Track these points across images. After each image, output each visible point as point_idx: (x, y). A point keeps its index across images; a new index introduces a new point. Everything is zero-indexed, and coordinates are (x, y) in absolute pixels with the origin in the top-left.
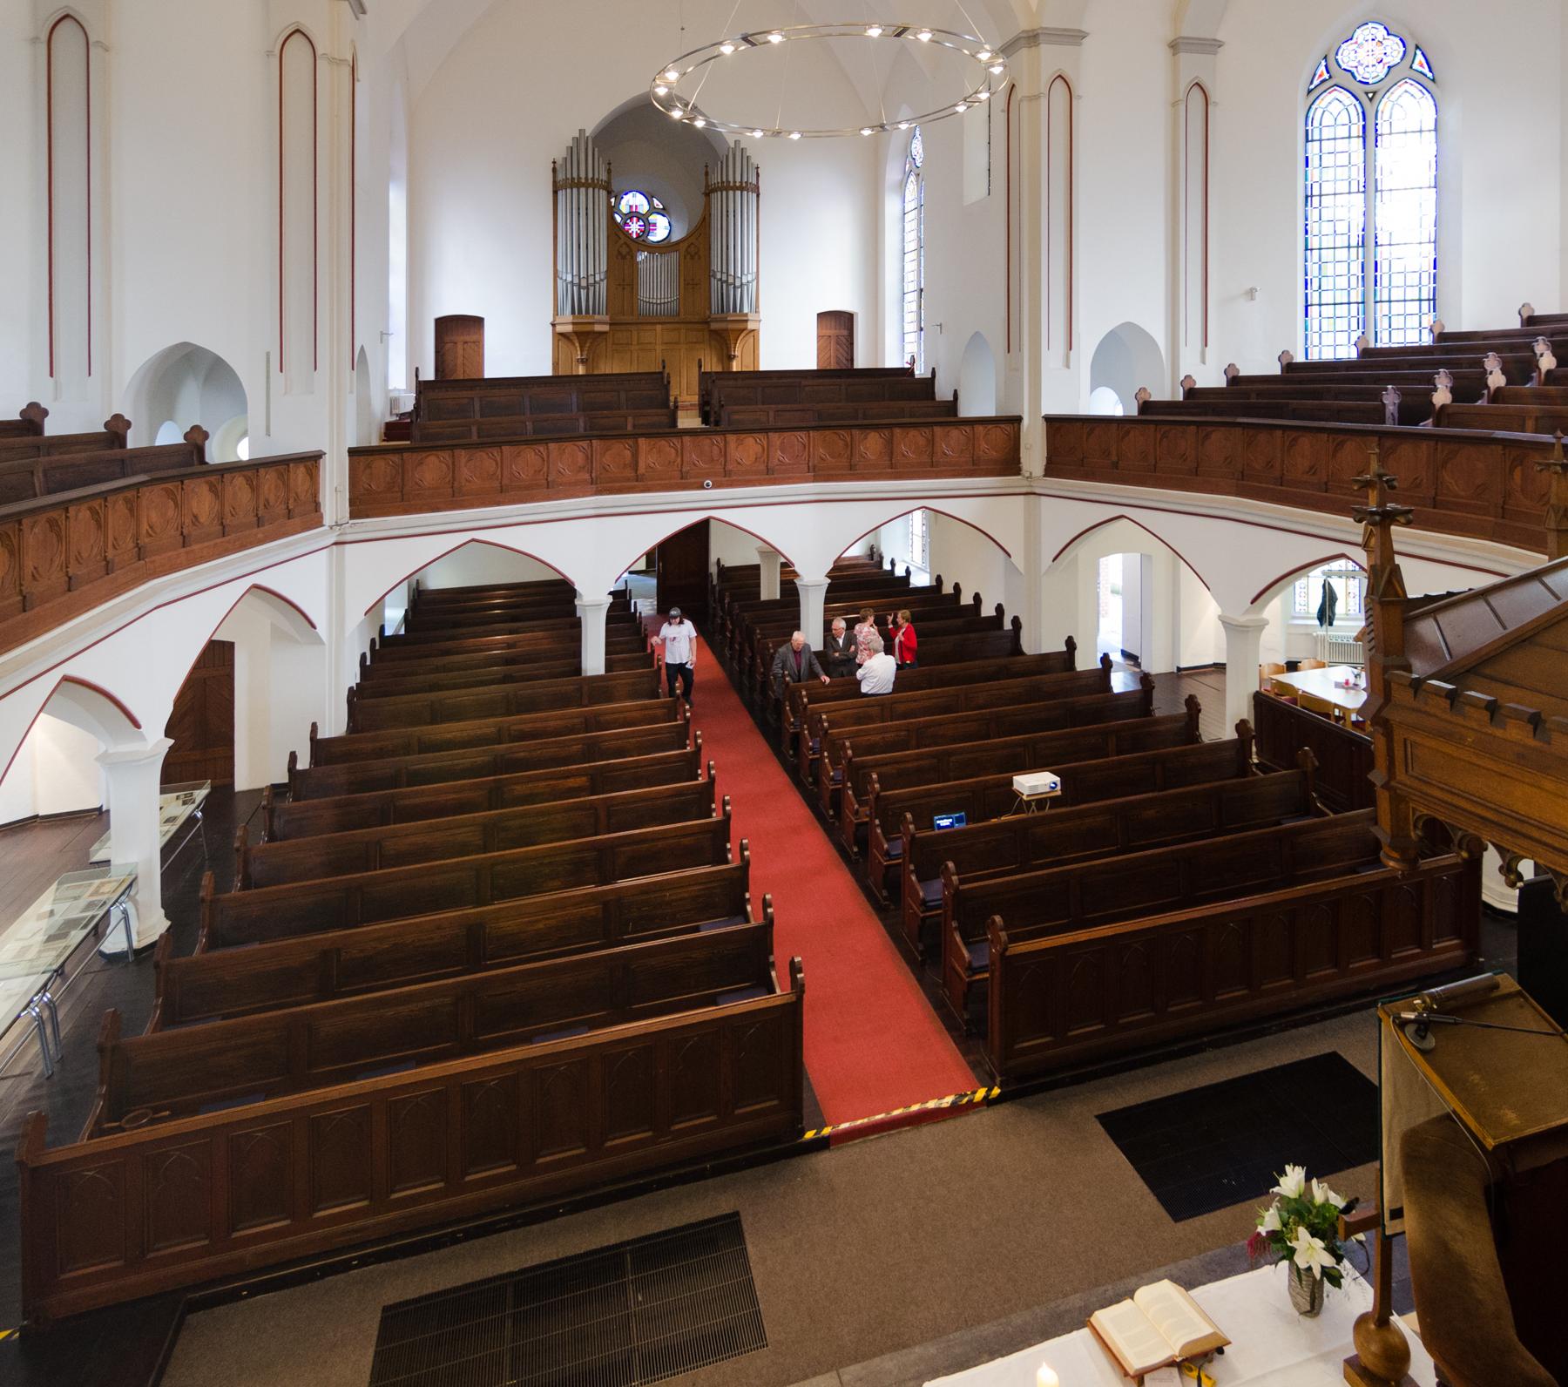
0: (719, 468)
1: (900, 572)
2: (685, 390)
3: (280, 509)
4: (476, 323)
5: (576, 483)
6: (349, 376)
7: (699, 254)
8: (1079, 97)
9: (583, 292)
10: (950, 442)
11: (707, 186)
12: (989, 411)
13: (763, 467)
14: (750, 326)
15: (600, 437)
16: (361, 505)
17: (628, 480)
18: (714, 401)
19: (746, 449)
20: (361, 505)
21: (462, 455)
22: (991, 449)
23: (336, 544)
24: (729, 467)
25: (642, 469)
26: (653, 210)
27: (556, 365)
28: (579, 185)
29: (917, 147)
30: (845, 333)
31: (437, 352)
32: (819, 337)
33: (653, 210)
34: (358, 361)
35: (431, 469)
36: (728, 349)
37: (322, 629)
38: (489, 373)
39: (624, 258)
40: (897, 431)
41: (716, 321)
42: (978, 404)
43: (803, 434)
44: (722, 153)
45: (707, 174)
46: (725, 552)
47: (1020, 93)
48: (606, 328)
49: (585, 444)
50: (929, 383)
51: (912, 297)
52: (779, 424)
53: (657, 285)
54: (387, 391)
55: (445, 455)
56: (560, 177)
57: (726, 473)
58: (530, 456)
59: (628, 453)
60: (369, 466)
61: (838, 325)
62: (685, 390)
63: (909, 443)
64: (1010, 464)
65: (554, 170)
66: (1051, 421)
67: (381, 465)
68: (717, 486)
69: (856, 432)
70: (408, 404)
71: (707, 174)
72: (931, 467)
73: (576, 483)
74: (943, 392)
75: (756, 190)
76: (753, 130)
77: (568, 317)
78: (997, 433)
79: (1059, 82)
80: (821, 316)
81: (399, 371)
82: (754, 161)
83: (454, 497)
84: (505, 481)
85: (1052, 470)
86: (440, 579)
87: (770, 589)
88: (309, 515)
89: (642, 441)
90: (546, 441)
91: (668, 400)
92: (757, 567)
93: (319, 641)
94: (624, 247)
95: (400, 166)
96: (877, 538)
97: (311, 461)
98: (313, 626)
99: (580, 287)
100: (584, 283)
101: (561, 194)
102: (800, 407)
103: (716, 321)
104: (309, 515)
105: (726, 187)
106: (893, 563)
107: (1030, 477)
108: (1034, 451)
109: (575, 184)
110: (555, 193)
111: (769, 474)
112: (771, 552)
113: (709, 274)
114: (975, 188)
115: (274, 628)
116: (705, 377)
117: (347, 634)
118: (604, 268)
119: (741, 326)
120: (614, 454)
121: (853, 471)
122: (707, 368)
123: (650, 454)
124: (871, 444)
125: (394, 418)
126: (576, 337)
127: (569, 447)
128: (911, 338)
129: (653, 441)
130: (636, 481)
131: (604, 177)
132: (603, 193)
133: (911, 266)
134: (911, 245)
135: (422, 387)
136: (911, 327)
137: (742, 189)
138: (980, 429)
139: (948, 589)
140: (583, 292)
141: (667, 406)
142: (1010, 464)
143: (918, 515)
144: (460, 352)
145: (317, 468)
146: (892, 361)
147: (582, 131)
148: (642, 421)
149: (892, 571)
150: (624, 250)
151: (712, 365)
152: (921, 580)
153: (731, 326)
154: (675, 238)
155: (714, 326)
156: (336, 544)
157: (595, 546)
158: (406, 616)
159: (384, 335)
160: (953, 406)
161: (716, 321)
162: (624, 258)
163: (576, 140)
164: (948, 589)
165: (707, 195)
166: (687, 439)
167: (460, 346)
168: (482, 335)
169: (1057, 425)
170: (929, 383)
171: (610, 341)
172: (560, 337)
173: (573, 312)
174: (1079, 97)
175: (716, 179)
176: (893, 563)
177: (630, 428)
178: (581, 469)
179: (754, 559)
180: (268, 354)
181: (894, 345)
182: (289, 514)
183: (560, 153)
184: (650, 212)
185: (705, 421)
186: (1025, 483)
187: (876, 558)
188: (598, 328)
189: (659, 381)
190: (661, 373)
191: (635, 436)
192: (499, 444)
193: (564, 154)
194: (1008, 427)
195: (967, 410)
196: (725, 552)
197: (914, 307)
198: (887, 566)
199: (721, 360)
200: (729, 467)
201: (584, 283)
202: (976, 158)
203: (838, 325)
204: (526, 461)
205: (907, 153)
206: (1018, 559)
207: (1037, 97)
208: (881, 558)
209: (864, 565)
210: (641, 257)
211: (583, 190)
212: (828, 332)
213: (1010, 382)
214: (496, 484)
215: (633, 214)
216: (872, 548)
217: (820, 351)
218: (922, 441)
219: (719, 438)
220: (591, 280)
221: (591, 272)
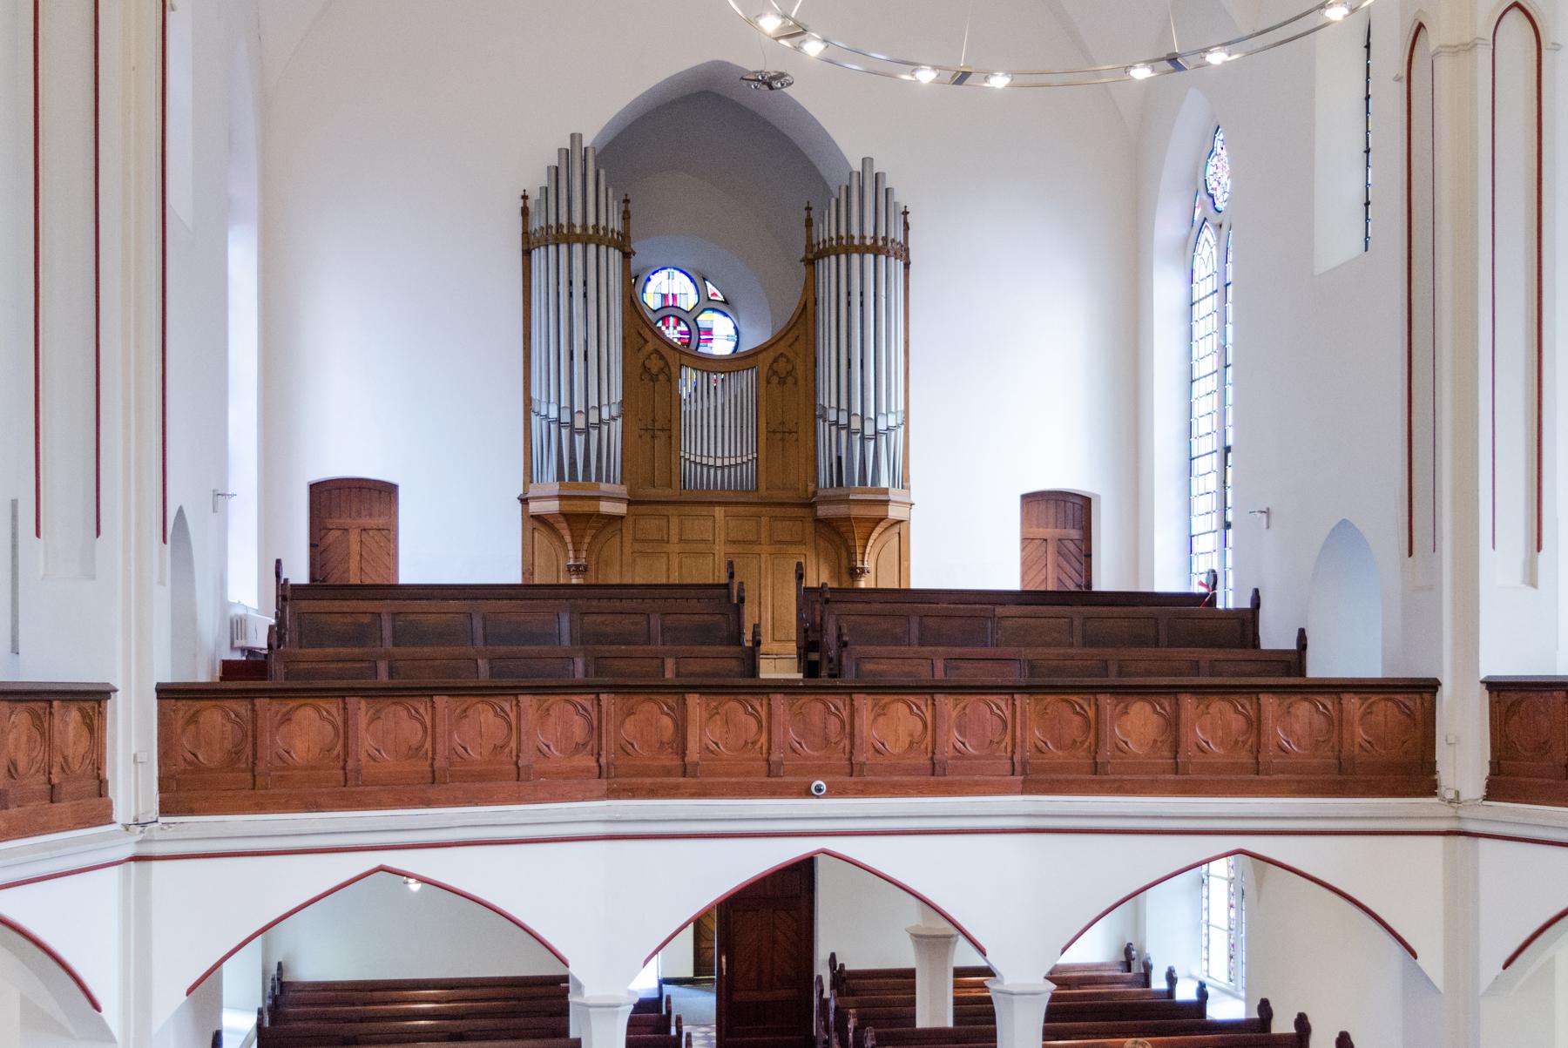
0: (839, 759)
1: (1185, 992)
2: (773, 613)
3: (37, 783)
4: (385, 492)
5: (567, 775)
6: (159, 556)
7: (793, 374)
8: (1557, 47)
9: (579, 440)
10: (1292, 725)
11: (810, 246)
12: (1372, 669)
13: (924, 760)
14: (894, 512)
15: (614, 689)
16: (183, 790)
17: (668, 772)
18: (830, 638)
19: (892, 725)
20: (183, 790)
21: (361, 709)
22: (1377, 743)
23: (136, 859)
24: (860, 757)
25: (693, 753)
26: (706, 304)
27: (528, 570)
28: (570, 239)
29: (1219, 174)
30: (1075, 534)
31: (313, 546)
32: (1026, 540)
33: (706, 304)
34: (173, 531)
35: (305, 731)
36: (851, 555)
37: (111, 1013)
38: (408, 574)
39: (654, 379)
40: (1188, 702)
41: (834, 511)
42: (1351, 645)
43: (1001, 700)
44: (835, 180)
45: (809, 223)
46: (848, 938)
47: (1433, 40)
48: (620, 509)
49: (586, 700)
50: (1247, 621)
51: (1207, 465)
52: (955, 678)
53: (716, 433)
54: (225, 605)
55: (332, 706)
56: (536, 223)
57: (853, 768)
58: (485, 718)
59: (667, 722)
60: (193, 719)
61: (1062, 517)
62: (773, 613)
63: (1211, 725)
64: (1413, 772)
65: (525, 212)
66: (1496, 687)
67: (214, 718)
68: (837, 791)
69: (1106, 701)
70: (259, 640)
71: (809, 223)
72: (1255, 773)
73: (567, 775)
74: (1275, 635)
75: (904, 253)
76: (914, 66)
77: (550, 485)
78: (1385, 710)
79: (1515, 14)
80: (1029, 499)
81: (244, 581)
82: (901, 198)
83: (345, 785)
84: (440, 763)
85: (1500, 786)
86: (323, 960)
87: (934, 1009)
88: (87, 800)
89: (693, 700)
90: (514, 691)
91: (740, 633)
92: (910, 974)
93: (105, 1034)
94: (654, 359)
95: (246, 191)
96: (1137, 922)
97: (93, 699)
98: (96, 1006)
99: (573, 431)
100: (580, 423)
101: (537, 256)
102: (990, 651)
103: (828, 501)
104: (87, 800)
105: (846, 247)
106: (1171, 978)
107: (1456, 800)
108: (1464, 745)
109: (562, 236)
110: (527, 253)
111: (935, 773)
112: (942, 930)
113: (815, 414)
114: (1337, 238)
115: (25, 1003)
116: (809, 598)
117: (155, 1028)
118: (617, 395)
119: (875, 512)
120: (645, 722)
121: (1100, 774)
122: (811, 581)
123: (710, 726)
124: (1137, 725)
125: (238, 656)
126: (563, 522)
127: (558, 705)
128: (1206, 543)
129: (714, 701)
130: (681, 775)
131: (616, 224)
132: (615, 256)
133: (1205, 405)
134: (1206, 365)
135: (287, 594)
136: (1205, 523)
137: (876, 251)
138: (1352, 703)
139: (1283, 1025)
140: (579, 440)
141: (737, 639)
142: (1413, 772)
143: (1220, 868)
144: (355, 547)
145: (101, 714)
146: (1167, 578)
147: (575, 138)
148: (694, 666)
149: (1170, 993)
150: (655, 365)
151: (819, 575)
152: (1226, 1008)
153: (856, 511)
154: (750, 343)
155: (823, 511)
156: (136, 859)
157: (609, 893)
158: (259, 1026)
159: (220, 496)
160: (1295, 659)
161: (828, 501)
162: (654, 379)
163: (566, 154)
164: (1283, 1025)
165: (811, 262)
166: (778, 700)
167: (354, 537)
168: (393, 514)
169: (1510, 697)
170: (1247, 621)
171: (628, 537)
172: (536, 523)
173: (560, 477)
174: (1557, 47)
175: (826, 231)
176: (1171, 978)
177: (669, 675)
178: (579, 748)
179: (902, 955)
180: (14, 504)
181: (1170, 548)
182: (53, 794)
183: (535, 180)
184: (700, 308)
185: (810, 669)
186: (1448, 811)
187: (1137, 968)
188: (606, 507)
189: (725, 601)
190: (726, 586)
191: (681, 689)
192: (428, 692)
193: (543, 180)
194: (1413, 701)
195: (1318, 667)
196: (851, 937)
197: (1212, 482)
198: (1159, 983)
199: (835, 574)
200: (860, 757)
201: (580, 423)
202: (1338, 182)
203: (1062, 517)
204: (480, 726)
205: (1200, 188)
206: (1431, 961)
207: (1470, 47)
208: (1148, 968)
209: (1114, 980)
210: (688, 381)
211: (578, 248)
212: (1050, 532)
213: (1417, 607)
214: (425, 766)
215: (670, 310)
216: (1128, 950)
217: (1024, 574)
218: (1237, 723)
219: (838, 701)
220: (594, 419)
221: (593, 402)
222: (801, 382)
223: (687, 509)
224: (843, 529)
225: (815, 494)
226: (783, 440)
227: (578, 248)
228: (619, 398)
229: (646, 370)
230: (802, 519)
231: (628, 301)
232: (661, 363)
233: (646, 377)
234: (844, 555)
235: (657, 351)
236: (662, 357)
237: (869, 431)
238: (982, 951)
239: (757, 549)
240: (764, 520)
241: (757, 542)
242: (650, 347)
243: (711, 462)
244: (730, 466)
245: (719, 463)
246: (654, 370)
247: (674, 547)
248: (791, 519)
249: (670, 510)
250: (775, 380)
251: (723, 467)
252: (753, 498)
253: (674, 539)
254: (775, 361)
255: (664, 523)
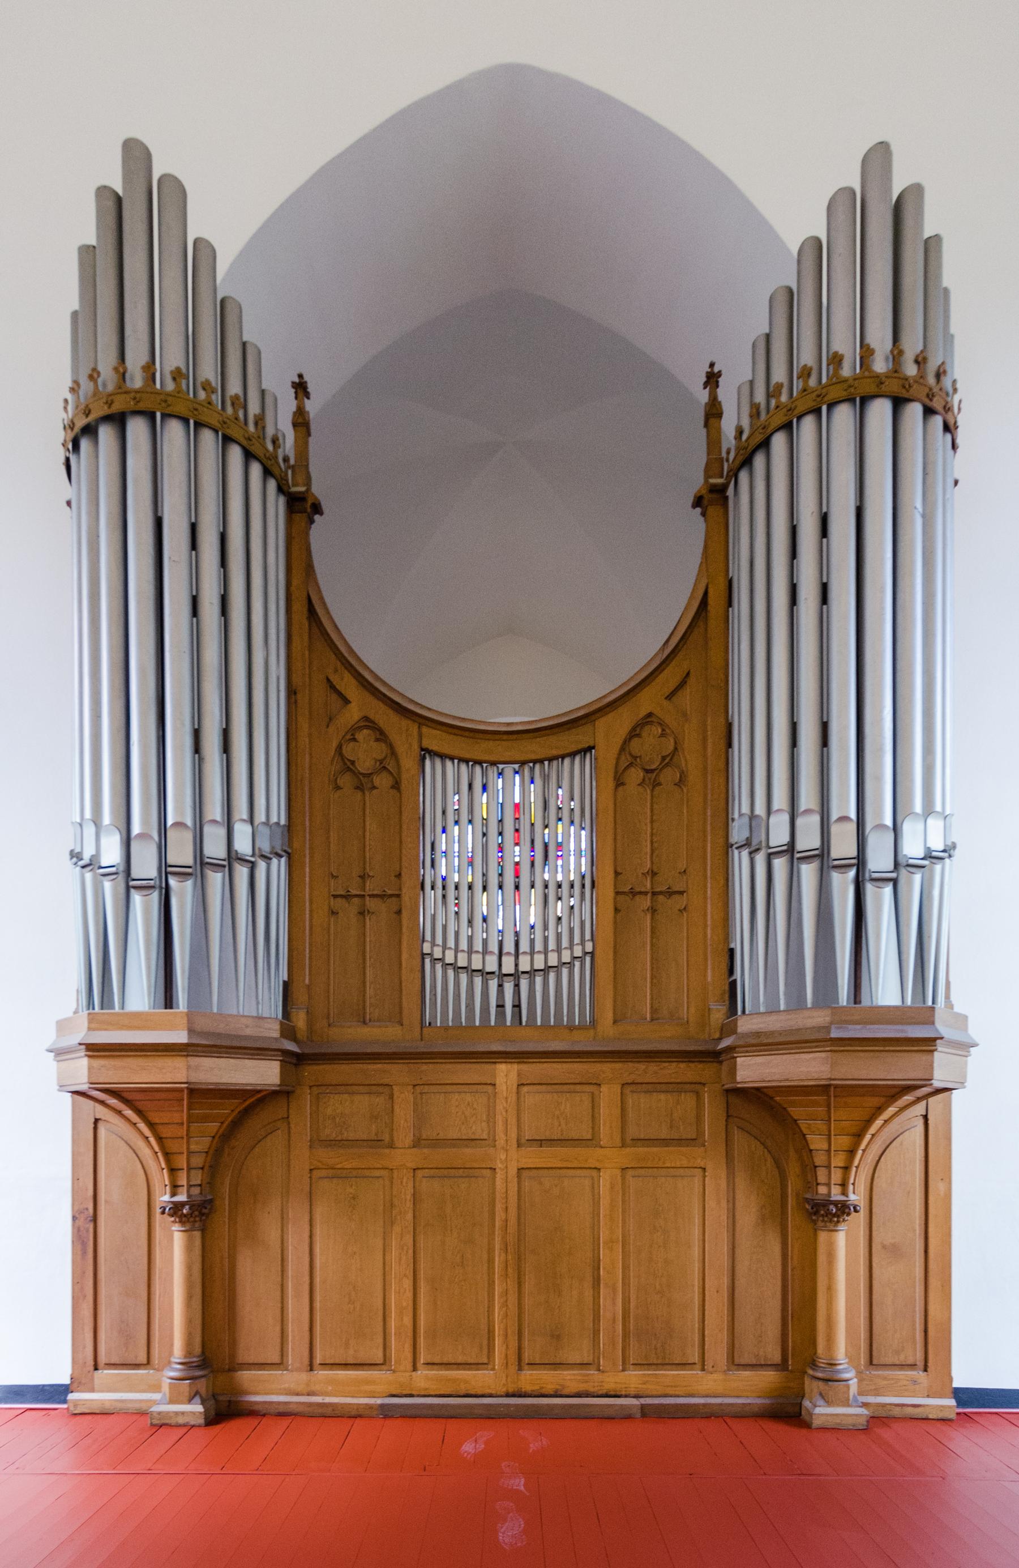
39: (363, 783)
150: (365, 753)
155: (752, 1070)
162: (363, 783)
222: (694, 777)
223: (430, 1071)
224: (795, 1112)
225: (728, 1029)
226: (653, 910)
227: (174, 433)
228: (279, 815)
229: (348, 767)
230: (695, 1088)
231: (300, 607)
232: (379, 750)
233: (346, 781)
234: (793, 1169)
235: (368, 723)
236: (381, 736)
237: (879, 860)
238: (68, 460)
239: (591, 1156)
240: (608, 1095)
241: (591, 1141)
242: (353, 714)
243: (491, 965)
244: (532, 973)
245: (508, 967)
246: (365, 764)
247: (404, 1157)
248: (676, 1087)
249: (396, 1072)
250: (635, 775)
251: (516, 976)
252: (583, 1042)
253: (404, 1137)
254: (634, 733)
255: (380, 1101)
